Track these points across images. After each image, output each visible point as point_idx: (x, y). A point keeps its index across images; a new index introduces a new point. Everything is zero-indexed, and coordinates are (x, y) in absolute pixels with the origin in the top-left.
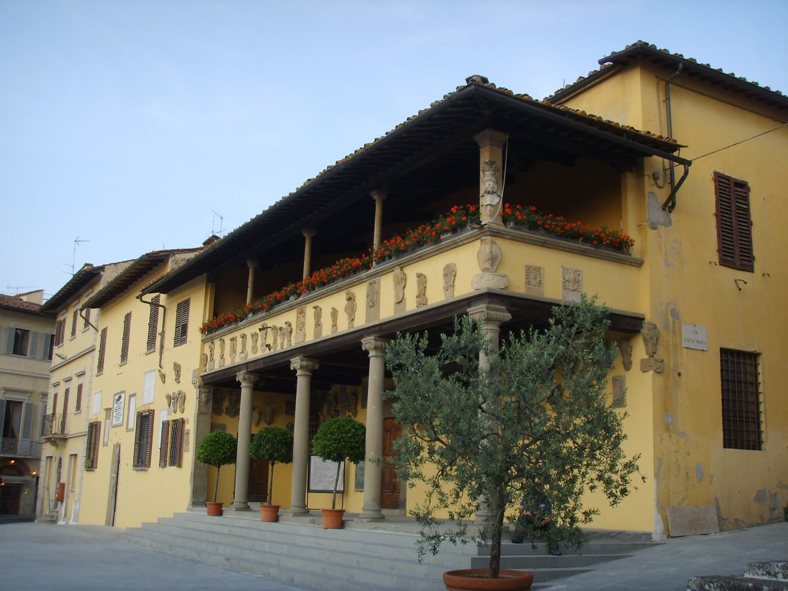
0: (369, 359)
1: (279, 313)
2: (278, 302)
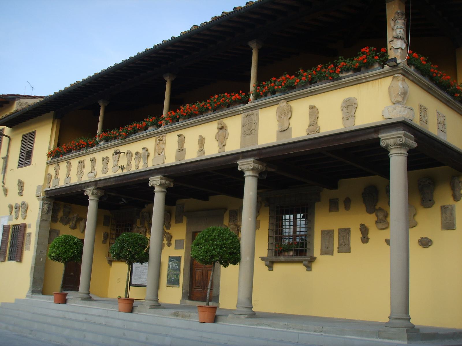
0: (244, 178)
1: (198, 124)
2: (135, 132)
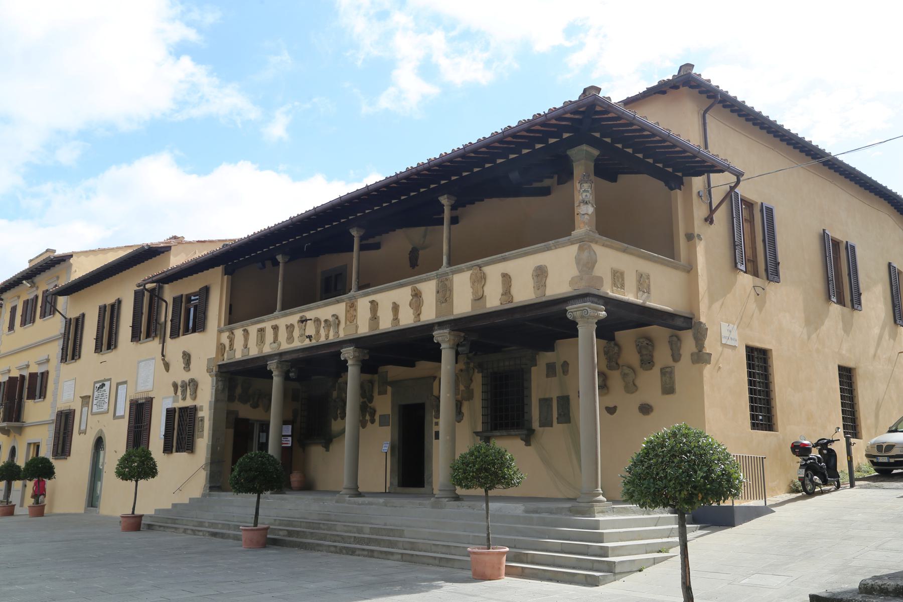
0: (441, 351)
